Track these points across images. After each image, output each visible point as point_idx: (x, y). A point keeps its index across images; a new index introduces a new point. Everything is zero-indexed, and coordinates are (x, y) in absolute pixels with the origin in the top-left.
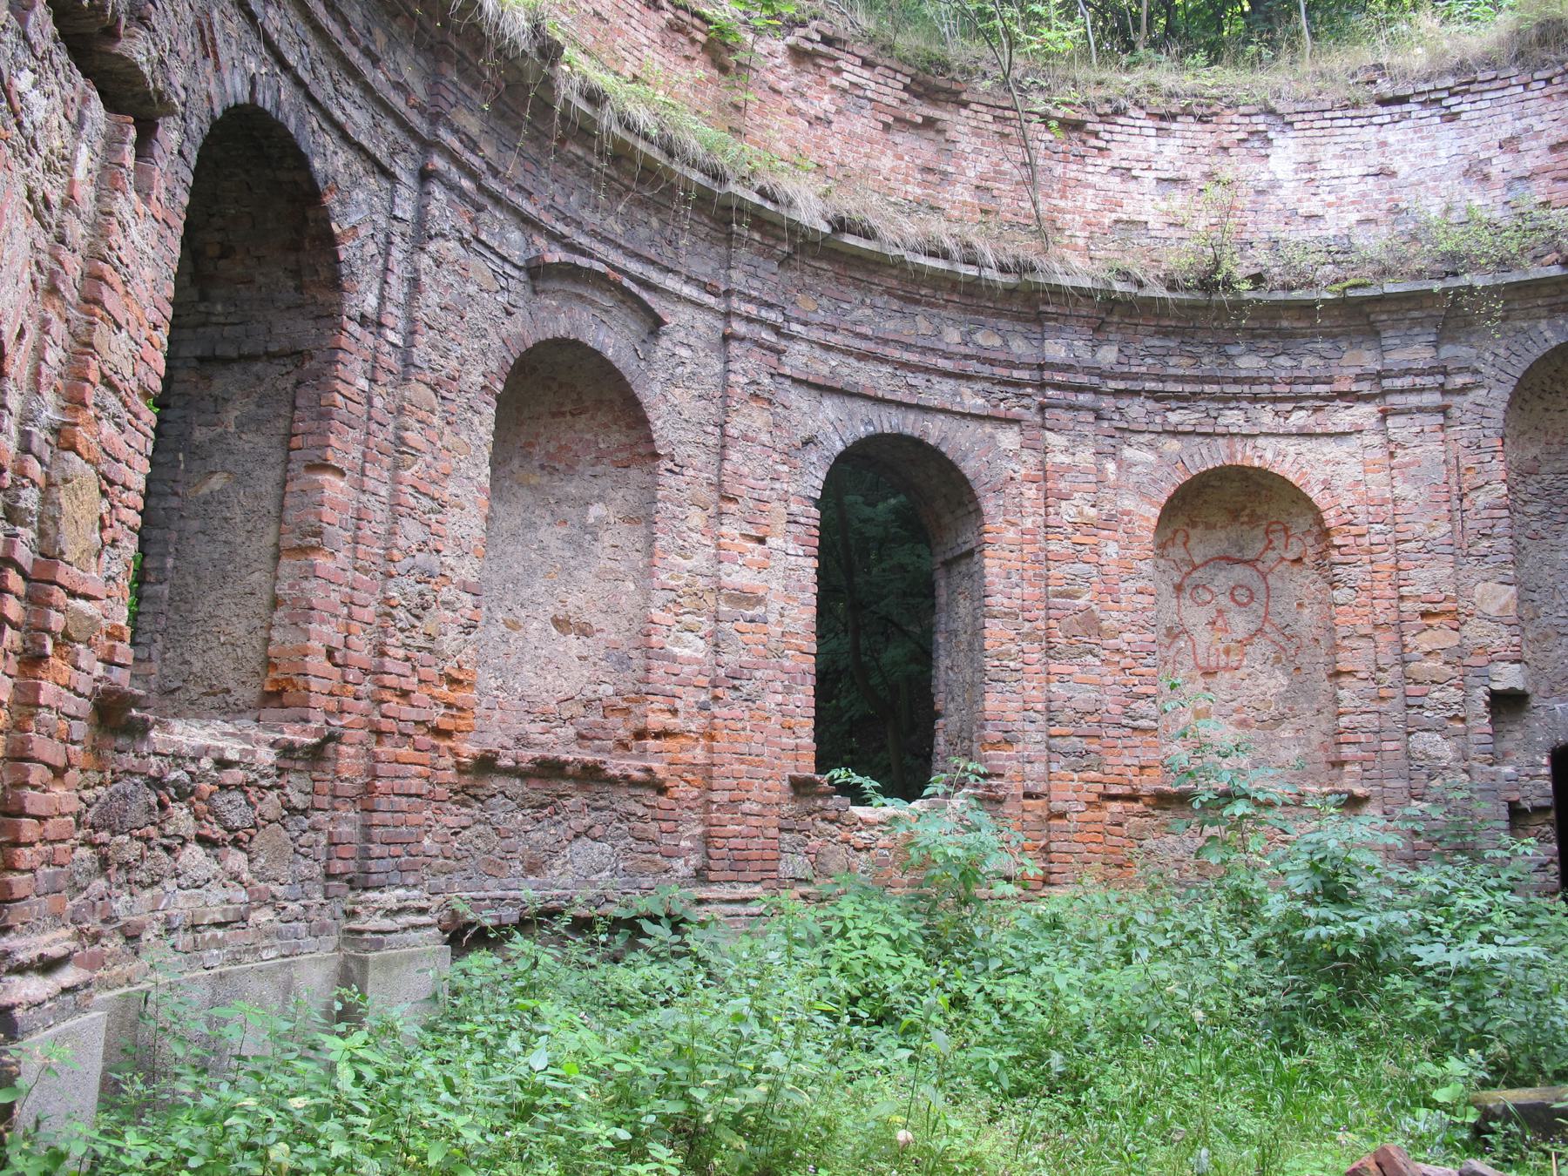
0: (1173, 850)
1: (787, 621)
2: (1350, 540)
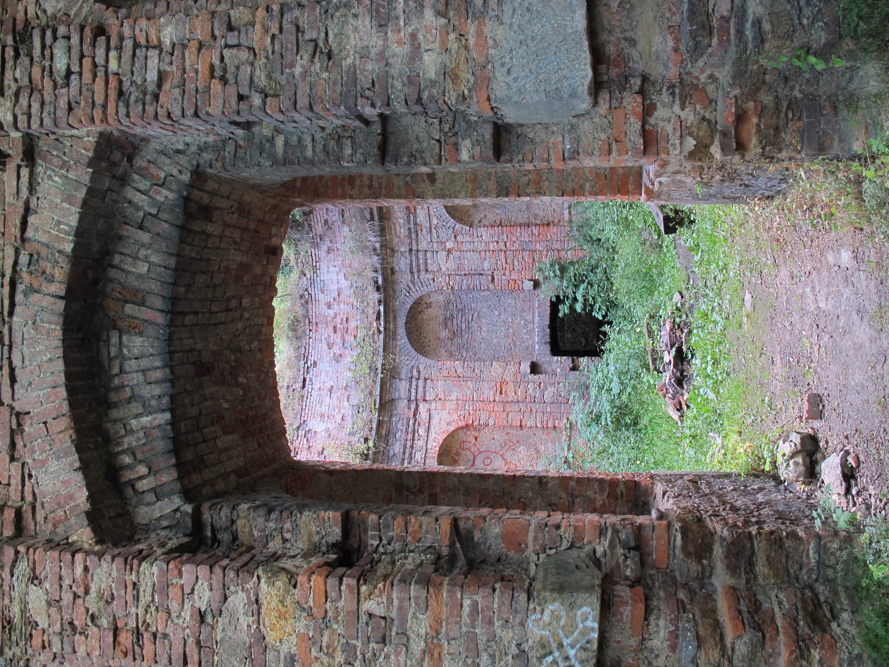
2: (471, 417)
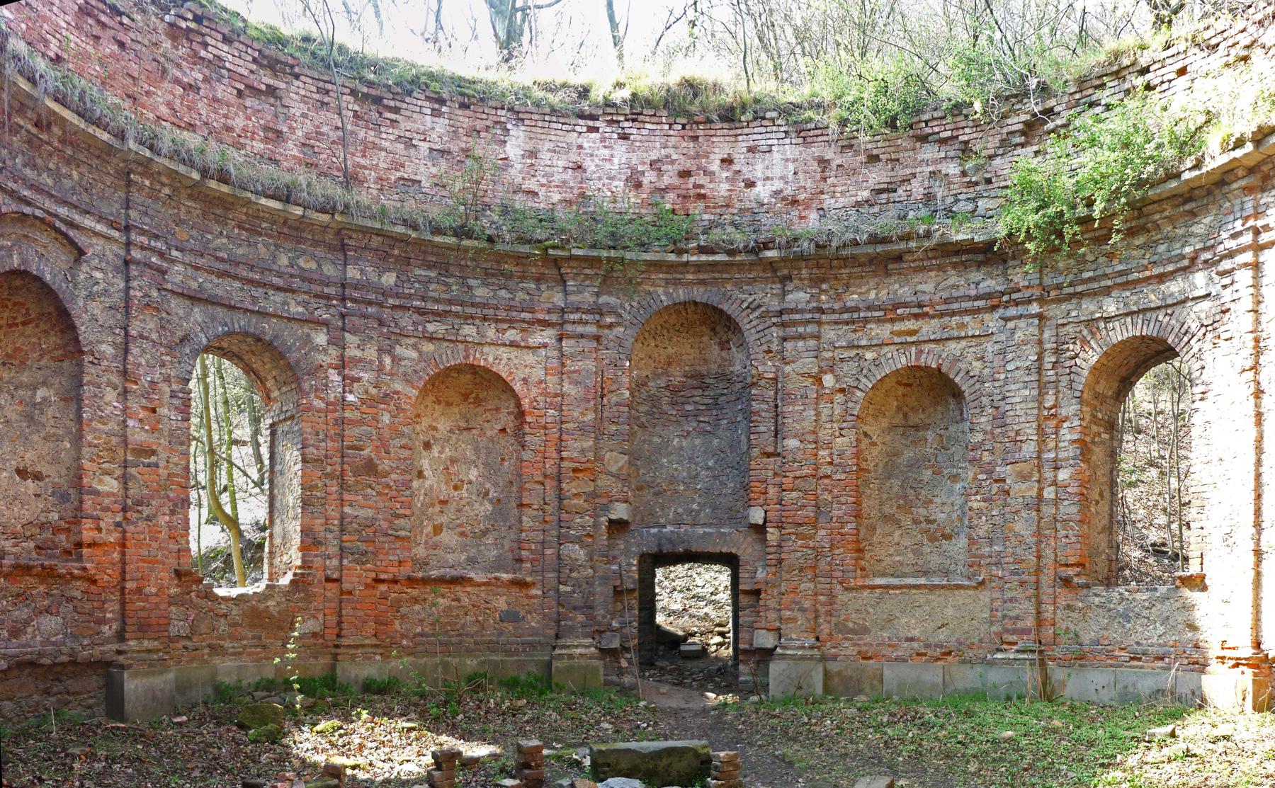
0: (418, 613)
1: (171, 466)
